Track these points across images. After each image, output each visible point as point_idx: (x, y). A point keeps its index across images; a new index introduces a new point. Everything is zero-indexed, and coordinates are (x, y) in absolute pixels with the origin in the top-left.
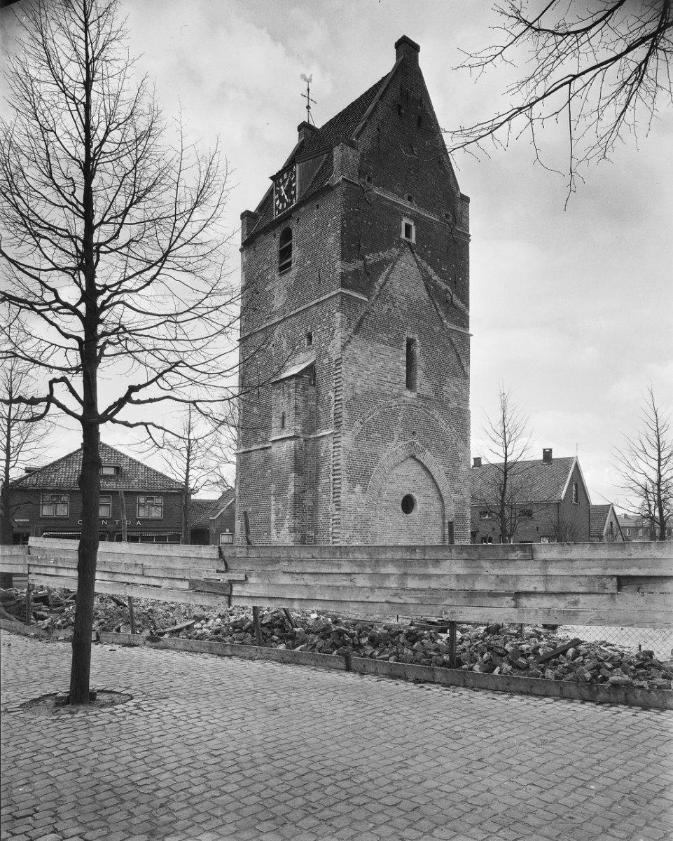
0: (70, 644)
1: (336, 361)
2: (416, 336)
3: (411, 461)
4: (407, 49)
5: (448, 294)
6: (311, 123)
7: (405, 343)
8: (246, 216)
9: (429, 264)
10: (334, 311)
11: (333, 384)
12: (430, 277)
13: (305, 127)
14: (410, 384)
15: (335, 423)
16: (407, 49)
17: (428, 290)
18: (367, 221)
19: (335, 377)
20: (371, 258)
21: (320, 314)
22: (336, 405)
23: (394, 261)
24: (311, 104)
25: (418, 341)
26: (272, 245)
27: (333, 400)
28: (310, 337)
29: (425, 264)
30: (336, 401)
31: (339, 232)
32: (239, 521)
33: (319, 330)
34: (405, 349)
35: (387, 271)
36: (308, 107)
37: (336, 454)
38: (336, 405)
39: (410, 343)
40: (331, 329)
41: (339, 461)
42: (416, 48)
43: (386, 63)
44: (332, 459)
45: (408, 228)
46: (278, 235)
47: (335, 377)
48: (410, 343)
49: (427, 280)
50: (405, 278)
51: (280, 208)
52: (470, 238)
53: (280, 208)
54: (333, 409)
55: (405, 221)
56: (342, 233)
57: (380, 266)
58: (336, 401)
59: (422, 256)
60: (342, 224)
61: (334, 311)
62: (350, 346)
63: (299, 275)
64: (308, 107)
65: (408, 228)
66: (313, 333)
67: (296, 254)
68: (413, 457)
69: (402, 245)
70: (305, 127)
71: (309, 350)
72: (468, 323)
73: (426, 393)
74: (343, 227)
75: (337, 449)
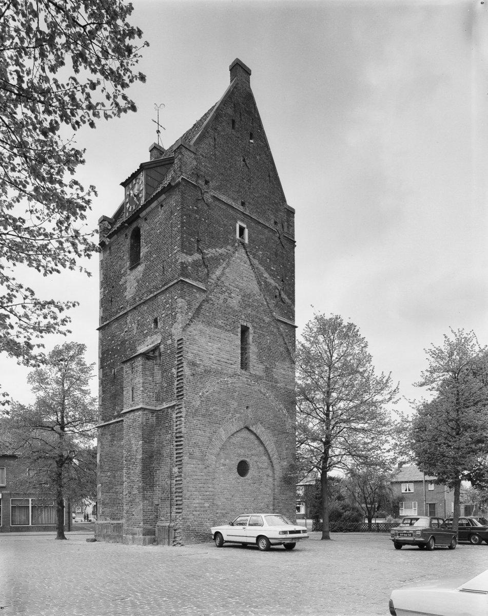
0: (400, 515)
1: (178, 341)
2: (249, 325)
3: (245, 434)
4: (239, 70)
5: (277, 291)
6: (160, 145)
7: (239, 330)
8: (104, 219)
9: (260, 264)
10: (176, 297)
11: (176, 362)
12: (261, 275)
13: (155, 149)
14: (244, 365)
15: (178, 396)
16: (239, 70)
17: (259, 283)
18: (205, 219)
19: (177, 356)
20: (210, 252)
21: (164, 301)
22: (178, 380)
23: (229, 256)
24: (160, 129)
25: (251, 328)
26: (125, 243)
27: (175, 376)
28: (156, 321)
29: (256, 262)
30: (178, 377)
31: (179, 226)
32: (100, 485)
33: (163, 316)
34: (239, 335)
35: (224, 265)
36: (158, 132)
37: (178, 423)
38: (178, 380)
39: (245, 330)
40: (173, 314)
41: (181, 429)
42: (248, 72)
43: (221, 85)
44: (175, 428)
45: (242, 230)
46: (130, 235)
47: (177, 356)
48: (245, 330)
49: (259, 277)
50: (239, 274)
51: (130, 210)
52: (296, 244)
53: (130, 210)
54: (176, 383)
55: (239, 224)
56: (182, 227)
57: (216, 260)
58: (178, 377)
59: (255, 256)
60: (182, 220)
61: (176, 297)
62: (190, 329)
63: (148, 268)
64: (158, 132)
65: (242, 230)
66: (159, 318)
67: (144, 251)
68: (247, 428)
69: (236, 244)
70: (155, 149)
71: (156, 333)
72: (294, 316)
73: (258, 373)
74: (182, 223)
75: (179, 419)
